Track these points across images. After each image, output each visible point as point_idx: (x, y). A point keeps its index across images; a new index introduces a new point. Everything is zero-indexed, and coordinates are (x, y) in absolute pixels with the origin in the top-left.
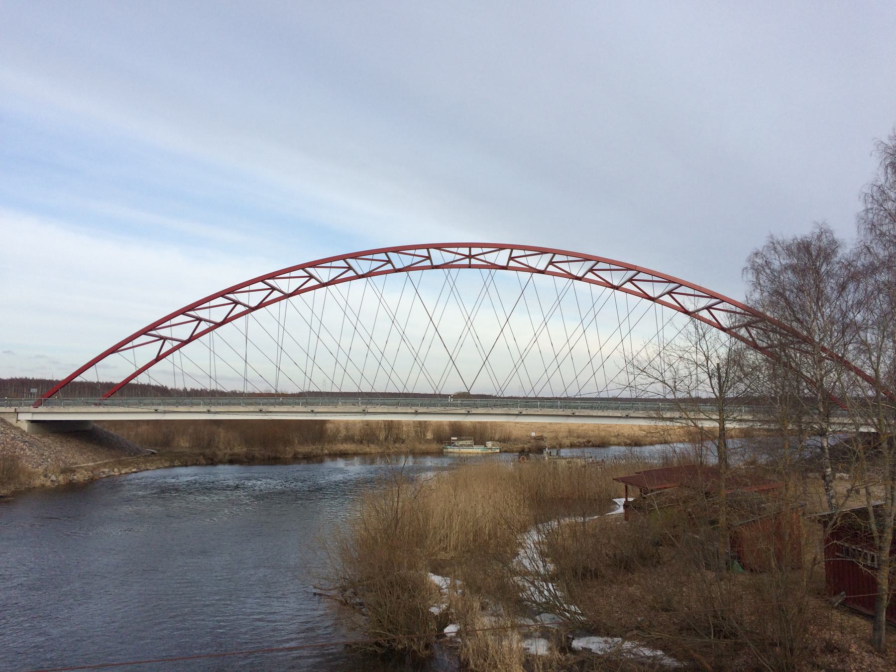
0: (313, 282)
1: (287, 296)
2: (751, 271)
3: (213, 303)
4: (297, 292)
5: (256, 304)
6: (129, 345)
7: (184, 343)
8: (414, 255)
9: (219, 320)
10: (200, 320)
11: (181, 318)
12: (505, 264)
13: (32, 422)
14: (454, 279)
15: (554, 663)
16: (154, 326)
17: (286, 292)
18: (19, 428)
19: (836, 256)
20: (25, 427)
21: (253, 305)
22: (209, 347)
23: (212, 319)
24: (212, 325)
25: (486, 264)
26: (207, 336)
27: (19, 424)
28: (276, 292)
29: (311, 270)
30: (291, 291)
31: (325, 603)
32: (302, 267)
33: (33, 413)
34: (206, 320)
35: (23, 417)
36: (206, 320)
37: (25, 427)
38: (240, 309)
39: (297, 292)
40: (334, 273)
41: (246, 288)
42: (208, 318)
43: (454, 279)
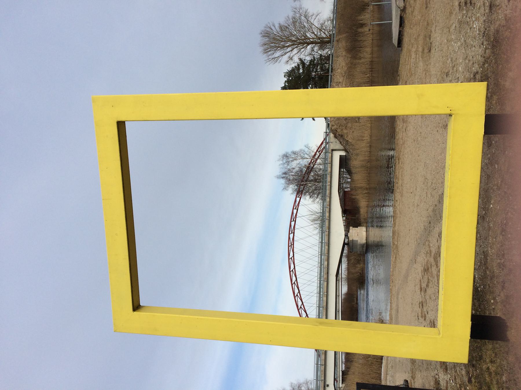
0: (298, 295)
1: (297, 280)
4: (305, 312)
8: (294, 289)
12: (299, 198)
13: (342, 383)
14: (305, 251)
15: (391, 153)
18: (344, 387)
20: (344, 385)
25: (344, 260)
27: (343, 387)
29: (299, 307)
30: (305, 313)
31: (318, 230)
32: (298, 310)
33: (339, 382)
35: (341, 386)
39: (305, 312)
40: (299, 300)
41: (301, 315)
43: (305, 251)
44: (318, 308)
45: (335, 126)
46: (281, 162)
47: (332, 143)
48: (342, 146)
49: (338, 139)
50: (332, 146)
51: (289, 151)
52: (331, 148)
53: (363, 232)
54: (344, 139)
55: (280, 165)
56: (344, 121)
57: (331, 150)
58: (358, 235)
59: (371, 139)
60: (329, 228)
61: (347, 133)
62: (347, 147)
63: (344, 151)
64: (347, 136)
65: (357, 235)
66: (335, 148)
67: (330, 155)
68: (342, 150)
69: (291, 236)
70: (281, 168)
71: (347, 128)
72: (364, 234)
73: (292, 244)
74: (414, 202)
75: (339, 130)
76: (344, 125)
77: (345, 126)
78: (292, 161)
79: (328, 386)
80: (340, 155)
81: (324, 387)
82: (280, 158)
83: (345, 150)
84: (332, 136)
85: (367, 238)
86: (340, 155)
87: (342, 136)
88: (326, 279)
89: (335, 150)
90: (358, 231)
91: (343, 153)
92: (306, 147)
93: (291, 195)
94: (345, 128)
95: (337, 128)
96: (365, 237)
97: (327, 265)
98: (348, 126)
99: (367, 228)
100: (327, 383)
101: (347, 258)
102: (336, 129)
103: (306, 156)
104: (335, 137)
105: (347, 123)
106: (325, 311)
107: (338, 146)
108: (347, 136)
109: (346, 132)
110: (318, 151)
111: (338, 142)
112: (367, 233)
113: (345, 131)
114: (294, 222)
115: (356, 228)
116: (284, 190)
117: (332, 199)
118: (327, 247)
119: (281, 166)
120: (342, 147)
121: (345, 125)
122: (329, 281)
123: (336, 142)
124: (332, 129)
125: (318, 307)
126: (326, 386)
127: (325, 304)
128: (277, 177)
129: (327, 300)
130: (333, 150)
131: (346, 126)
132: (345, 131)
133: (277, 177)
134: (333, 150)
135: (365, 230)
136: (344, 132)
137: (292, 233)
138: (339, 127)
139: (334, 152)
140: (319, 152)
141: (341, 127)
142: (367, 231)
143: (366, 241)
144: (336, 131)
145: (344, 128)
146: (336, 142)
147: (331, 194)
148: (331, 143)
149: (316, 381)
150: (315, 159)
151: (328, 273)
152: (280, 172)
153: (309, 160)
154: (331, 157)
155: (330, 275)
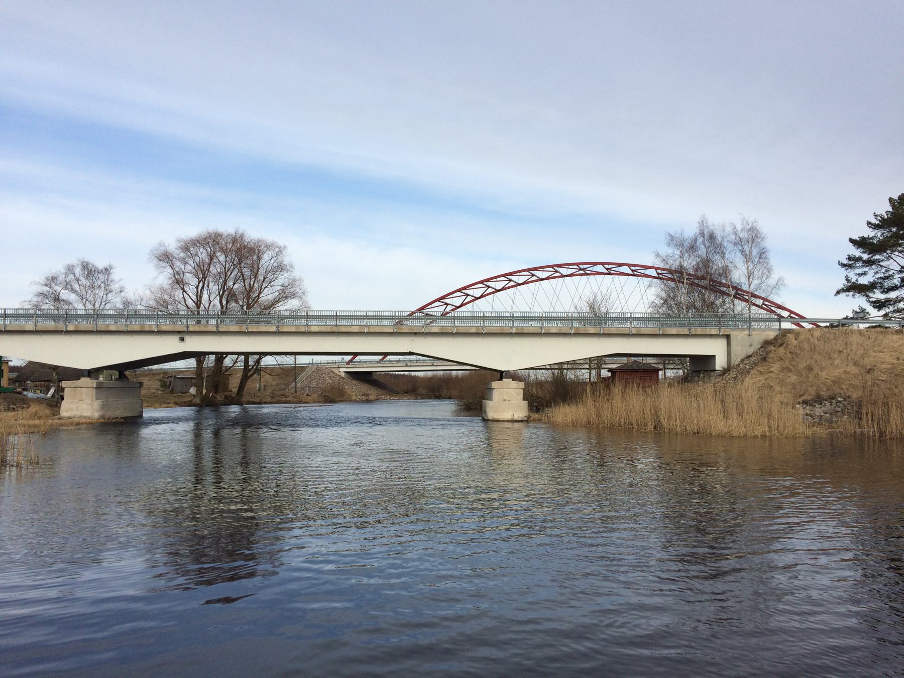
13: (346, 372)
20: (343, 375)
35: (342, 370)
44: (335, 314)
45: (795, 342)
46: (739, 228)
47: (749, 335)
48: (739, 360)
50: (738, 336)
51: (768, 243)
55: (733, 224)
57: (727, 333)
58: (505, 400)
59: (718, 436)
61: (772, 372)
62: (733, 374)
64: (761, 373)
65: (506, 398)
69: (626, 269)
71: (785, 371)
72: (507, 416)
75: (781, 350)
79: (182, 339)
80: (715, 356)
81: (179, 332)
82: (750, 223)
83: (725, 371)
84: (770, 335)
85: (498, 421)
86: (715, 356)
87: (764, 359)
88: (398, 331)
89: (729, 344)
90: (513, 402)
91: (720, 363)
92: (779, 280)
93: (654, 252)
94: (785, 365)
95: (790, 347)
96: (500, 417)
98: (790, 374)
101: (444, 377)
103: (755, 282)
104: (767, 343)
105: (799, 373)
106: (329, 331)
107: (740, 351)
108: (761, 373)
110: (791, 313)
111: (751, 351)
112: (508, 421)
113: (775, 367)
114: (657, 276)
115: (521, 396)
117: (597, 339)
118: (473, 330)
119: (729, 229)
120: (736, 360)
121: (794, 366)
122: (398, 338)
125: (307, 313)
126: (181, 336)
127: (344, 329)
128: (703, 221)
129: (404, 333)
130: (728, 337)
131: (790, 370)
132: (775, 367)
133: (703, 221)
134: (728, 337)
135: (516, 417)
136: (773, 365)
138: (790, 352)
140: (789, 316)
141: (789, 355)
142: (513, 421)
143: (490, 420)
144: (781, 345)
145: (787, 364)
147: (653, 338)
148: (747, 332)
154: (709, 333)
155: (412, 338)
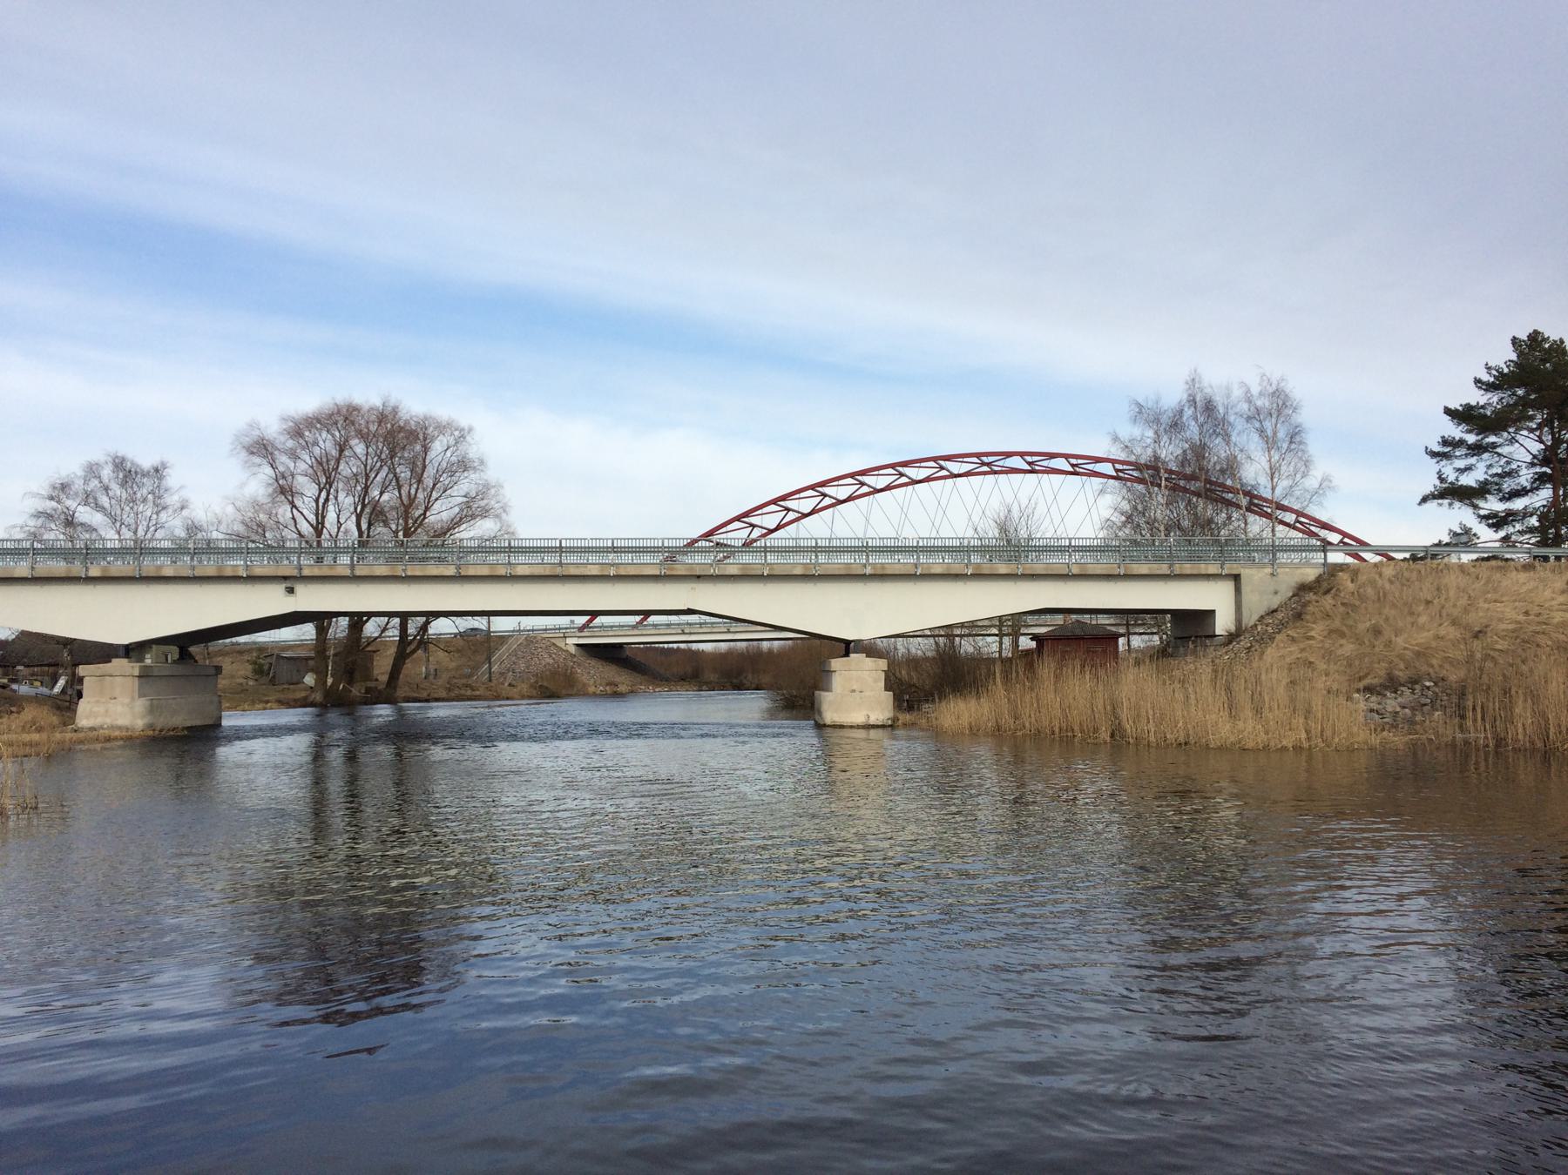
2: (110, 465)
3: (766, 510)
5: (845, 497)
6: (759, 512)
7: (772, 531)
9: (773, 526)
10: (788, 510)
11: (773, 508)
13: (578, 645)
16: (747, 514)
17: (914, 478)
19: (158, 472)
20: (573, 650)
21: (842, 498)
22: (932, 517)
23: (764, 525)
24: (765, 531)
26: (795, 525)
28: (865, 487)
34: (830, 497)
36: (830, 497)
37: (573, 650)
38: (827, 501)
41: (797, 496)
42: (796, 509)
45: (1351, 586)
46: (1255, 390)
47: (1272, 574)
48: (1255, 617)
49: (1290, 599)
50: (1253, 576)
51: (1304, 417)
52: (1247, 571)
53: (865, 713)
54: (1282, 625)
56: (1368, 624)
58: (854, 691)
60: (979, 576)
62: (1245, 642)
63: (1233, 629)
64: (1293, 640)
65: (855, 687)
66: (1245, 588)
67: (1213, 569)
68: (1239, 620)
69: (1061, 464)
70: (1228, 389)
72: (858, 718)
73: (1121, 474)
74: (1440, 625)
75: (1328, 601)
76: (1350, 622)
77: (1344, 629)
78: (1261, 431)
79: (291, 591)
80: (1213, 612)
81: (285, 578)
83: (1232, 637)
84: (1308, 575)
86: (1213, 612)
87: (1299, 616)
88: (668, 573)
89: (1238, 590)
90: (867, 693)
91: (1223, 623)
92: (1323, 480)
95: (1342, 595)
97: (727, 573)
98: (1343, 641)
99: (883, 726)
100: (300, 589)
101: (748, 651)
102: (1333, 591)
104: (1303, 588)
106: (547, 573)
107: (1256, 603)
109: (1312, 633)
111: (1275, 602)
112: (858, 727)
113: (1318, 630)
116: (1133, 406)
120: (1250, 619)
123: (1276, 593)
124: (1342, 571)
126: (289, 585)
127: (573, 571)
130: (1236, 578)
131: (1342, 635)
132: (1318, 630)
134: (1236, 578)
135: (873, 721)
137: (1117, 471)
138: (1343, 604)
139: (1227, 588)
141: (1342, 609)
143: (829, 726)
144: (1327, 592)
145: (1337, 623)
146: (1276, 593)
147: (1034, 580)
149: (811, 547)
150: (1269, 511)
151: (699, 578)
152: (1211, 387)
153: (1267, 494)
